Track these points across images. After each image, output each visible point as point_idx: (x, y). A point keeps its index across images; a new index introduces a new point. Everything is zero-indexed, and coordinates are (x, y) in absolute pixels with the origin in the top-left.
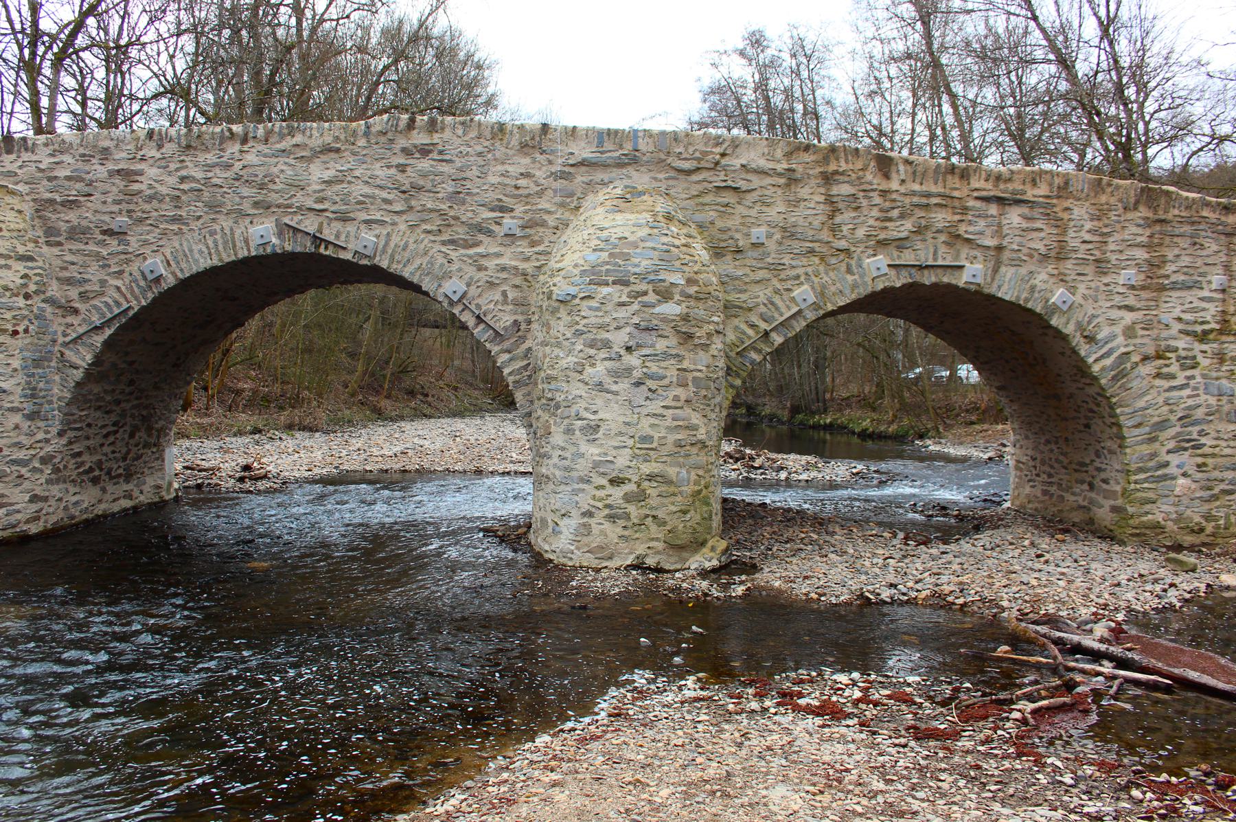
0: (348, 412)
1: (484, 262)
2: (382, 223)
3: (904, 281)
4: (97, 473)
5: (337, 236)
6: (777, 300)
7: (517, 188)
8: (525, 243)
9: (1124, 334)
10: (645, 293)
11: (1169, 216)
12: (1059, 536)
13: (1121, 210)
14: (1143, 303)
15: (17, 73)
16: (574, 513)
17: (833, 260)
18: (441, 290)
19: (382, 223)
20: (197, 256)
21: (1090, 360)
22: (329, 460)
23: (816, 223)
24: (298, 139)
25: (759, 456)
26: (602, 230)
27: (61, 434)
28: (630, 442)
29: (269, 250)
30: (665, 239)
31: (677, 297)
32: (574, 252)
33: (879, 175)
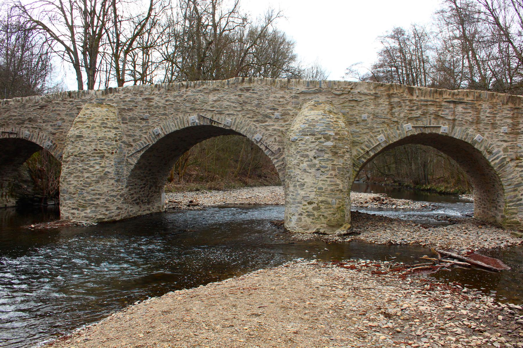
0: (233, 183)
1: (268, 128)
2: (233, 115)
3: (418, 132)
4: (138, 201)
5: (218, 119)
6: (372, 140)
7: (279, 102)
8: (282, 121)
9: (503, 151)
10: (321, 138)
11: (520, 107)
12: (480, 226)
13: (501, 105)
14: (511, 139)
15: (112, 58)
16: (296, 214)
17: (392, 125)
18: (254, 138)
19: (233, 115)
20: (171, 127)
21: (490, 161)
22: (222, 200)
23: (386, 112)
24: (205, 86)
25: (386, 199)
26: (306, 116)
27: (127, 187)
28: (315, 190)
29: (195, 124)
30: (328, 120)
31: (332, 140)
32: (298, 124)
33: (409, 94)
